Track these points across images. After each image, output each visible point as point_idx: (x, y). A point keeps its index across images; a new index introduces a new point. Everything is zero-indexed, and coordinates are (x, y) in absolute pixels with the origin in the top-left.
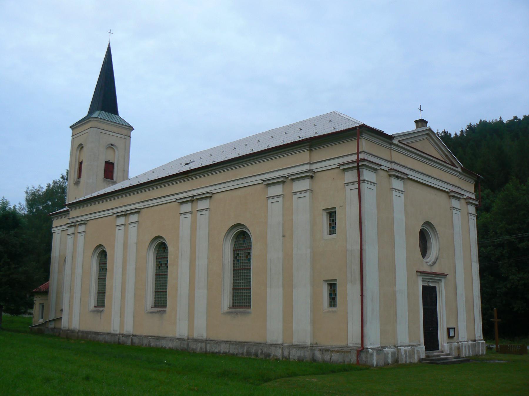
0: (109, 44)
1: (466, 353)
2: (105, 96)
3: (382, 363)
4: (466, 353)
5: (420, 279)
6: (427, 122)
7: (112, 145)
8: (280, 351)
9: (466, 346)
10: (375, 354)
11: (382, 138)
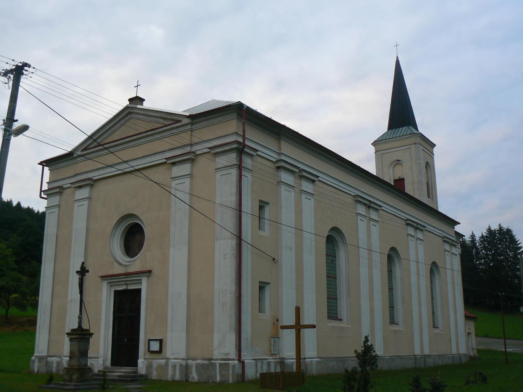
0: (397, 57)
1: (174, 375)
2: (401, 113)
3: (43, 370)
4: (174, 375)
5: (105, 285)
6: (144, 100)
7: (399, 161)
8: (65, 358)
9: (174, 367)
10: (37, 361)
11: (62, 160)
